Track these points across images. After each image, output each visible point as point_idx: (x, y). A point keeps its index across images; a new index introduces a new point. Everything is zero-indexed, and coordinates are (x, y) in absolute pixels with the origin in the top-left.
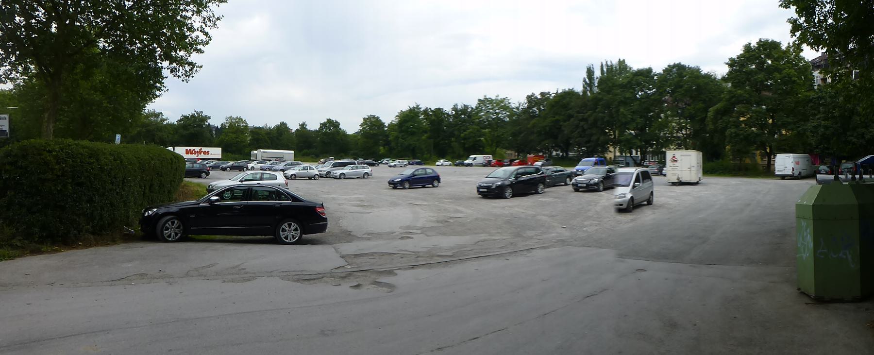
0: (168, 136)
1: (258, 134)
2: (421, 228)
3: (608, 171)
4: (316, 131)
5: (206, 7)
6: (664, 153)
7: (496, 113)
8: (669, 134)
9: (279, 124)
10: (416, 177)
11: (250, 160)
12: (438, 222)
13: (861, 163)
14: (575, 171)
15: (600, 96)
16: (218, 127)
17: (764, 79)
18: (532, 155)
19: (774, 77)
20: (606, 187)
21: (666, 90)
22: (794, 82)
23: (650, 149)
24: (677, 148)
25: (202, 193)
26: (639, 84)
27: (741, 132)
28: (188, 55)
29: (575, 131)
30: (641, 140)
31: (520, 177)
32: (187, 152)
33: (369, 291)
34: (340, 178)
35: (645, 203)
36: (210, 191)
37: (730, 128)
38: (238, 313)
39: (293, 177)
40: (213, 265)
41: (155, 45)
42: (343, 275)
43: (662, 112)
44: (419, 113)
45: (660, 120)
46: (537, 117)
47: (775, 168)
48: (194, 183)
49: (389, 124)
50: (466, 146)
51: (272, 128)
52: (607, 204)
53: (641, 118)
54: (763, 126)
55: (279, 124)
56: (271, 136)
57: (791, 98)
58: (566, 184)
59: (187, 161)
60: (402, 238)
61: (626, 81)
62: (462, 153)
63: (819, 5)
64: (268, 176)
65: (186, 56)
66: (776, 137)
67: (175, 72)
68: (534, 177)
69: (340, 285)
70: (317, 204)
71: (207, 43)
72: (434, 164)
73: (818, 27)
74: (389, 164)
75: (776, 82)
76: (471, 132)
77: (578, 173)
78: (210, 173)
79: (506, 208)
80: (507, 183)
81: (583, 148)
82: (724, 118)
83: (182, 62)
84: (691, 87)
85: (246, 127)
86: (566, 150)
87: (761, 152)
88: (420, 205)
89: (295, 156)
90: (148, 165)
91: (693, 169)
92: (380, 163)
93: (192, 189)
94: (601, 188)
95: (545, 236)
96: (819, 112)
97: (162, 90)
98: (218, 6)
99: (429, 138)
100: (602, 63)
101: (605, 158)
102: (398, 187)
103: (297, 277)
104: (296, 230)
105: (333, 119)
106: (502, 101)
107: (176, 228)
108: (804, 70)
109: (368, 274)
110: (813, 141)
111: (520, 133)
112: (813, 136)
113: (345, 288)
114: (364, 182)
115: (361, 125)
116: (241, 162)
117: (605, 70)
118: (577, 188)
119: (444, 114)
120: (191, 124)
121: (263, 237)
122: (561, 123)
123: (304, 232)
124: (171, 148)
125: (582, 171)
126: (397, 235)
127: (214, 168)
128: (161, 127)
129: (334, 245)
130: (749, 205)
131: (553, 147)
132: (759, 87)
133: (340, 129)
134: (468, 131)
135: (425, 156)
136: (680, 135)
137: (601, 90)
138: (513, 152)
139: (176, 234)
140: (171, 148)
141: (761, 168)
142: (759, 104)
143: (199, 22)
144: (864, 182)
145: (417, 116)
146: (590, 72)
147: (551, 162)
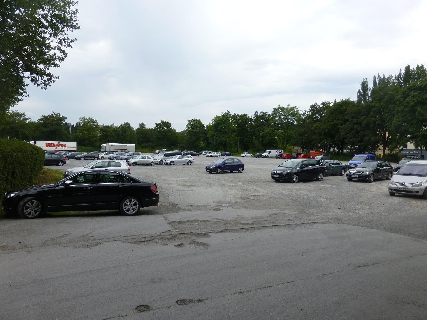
0: (30, 133)
1: (107, 131)
2: (229, 203)
3: (378, 166)
4: (152, 129)
5: (62, 31)
7: (286, 118)
9: (124, 124)
10: (226, 165)
11: (100, 151)
14: (349, 164)
15: (373, 104)
16: (73, 125)
18: (314, 151)
20: (375, 179)
25: (59, 178)
28: (46, 68)
29: (350, 133)
31: (304, 167)
32: (47, 145)
33: (189, 248)
34: (170, 165)
36: (65, 176)
38: (87, 272)
39: (135, 164)
40: (66, 235)
41: (18, 59)
42: (170, 237)
46: (319, 121)
48: (52, 170)
49: (207, 126)
50: (264, 142)
51: (118, 127)
52: (377, 192)
55: (124, 124)
56: (118, 133)
58: (341, 175)
59: (46, 153)
60: (215, 210)
62: (260, 148)
64: (114, 164)
65: (45, 68)
67: (35, 81)
68: (317, 167)
69: (167, 244)
70: (151, 184)
71: (63, 59)
72: (240, 156)
74: (207, 155)
76: (268, 132)
77: (351, 166)
78: (67, 162)
79: (293, 190)
80: (294, 171)
83: (41, 73)
85: (97, 126)
88: (229, 186)
89: (137, 148)
90: (11, 156)
92: (200, 154)
93: (50, 175)
94: (372, 179)
95: (323, 214)
97: (24, 95)
98: (72, 31)
99: (235, 136)
100: (375, 76)
101: (376, 155)
102: (213, 172)
103: (135, 240)
104: (135, 204)
105: (166, 120)
106: (292, 109)
107: (35, 207)
109: (189, 236)
111: (305, 134)
113: (171, 246)
114: (187, 168)
115: (187, 126)
116: (93, 153)
117: (377, 82)
118: (350, 178)
119: (248, 118)
120: (50, 122)
121: (110, 211)
122: (338, 127)
123: (141, 205)
124: (32, 143)
125: (355, 164)
126: (211, 208)
127: (70, 158)
128: (24, 125)
129: (165, 215)
133: (171, 128)
134: (265, 131)
137: (373, 99)
138: (299, 148)
139: (36, 212)
140: (32, 143)
143: (56, 42)
145: (227, 119)
146: (364, 85)
147: (329, 156)
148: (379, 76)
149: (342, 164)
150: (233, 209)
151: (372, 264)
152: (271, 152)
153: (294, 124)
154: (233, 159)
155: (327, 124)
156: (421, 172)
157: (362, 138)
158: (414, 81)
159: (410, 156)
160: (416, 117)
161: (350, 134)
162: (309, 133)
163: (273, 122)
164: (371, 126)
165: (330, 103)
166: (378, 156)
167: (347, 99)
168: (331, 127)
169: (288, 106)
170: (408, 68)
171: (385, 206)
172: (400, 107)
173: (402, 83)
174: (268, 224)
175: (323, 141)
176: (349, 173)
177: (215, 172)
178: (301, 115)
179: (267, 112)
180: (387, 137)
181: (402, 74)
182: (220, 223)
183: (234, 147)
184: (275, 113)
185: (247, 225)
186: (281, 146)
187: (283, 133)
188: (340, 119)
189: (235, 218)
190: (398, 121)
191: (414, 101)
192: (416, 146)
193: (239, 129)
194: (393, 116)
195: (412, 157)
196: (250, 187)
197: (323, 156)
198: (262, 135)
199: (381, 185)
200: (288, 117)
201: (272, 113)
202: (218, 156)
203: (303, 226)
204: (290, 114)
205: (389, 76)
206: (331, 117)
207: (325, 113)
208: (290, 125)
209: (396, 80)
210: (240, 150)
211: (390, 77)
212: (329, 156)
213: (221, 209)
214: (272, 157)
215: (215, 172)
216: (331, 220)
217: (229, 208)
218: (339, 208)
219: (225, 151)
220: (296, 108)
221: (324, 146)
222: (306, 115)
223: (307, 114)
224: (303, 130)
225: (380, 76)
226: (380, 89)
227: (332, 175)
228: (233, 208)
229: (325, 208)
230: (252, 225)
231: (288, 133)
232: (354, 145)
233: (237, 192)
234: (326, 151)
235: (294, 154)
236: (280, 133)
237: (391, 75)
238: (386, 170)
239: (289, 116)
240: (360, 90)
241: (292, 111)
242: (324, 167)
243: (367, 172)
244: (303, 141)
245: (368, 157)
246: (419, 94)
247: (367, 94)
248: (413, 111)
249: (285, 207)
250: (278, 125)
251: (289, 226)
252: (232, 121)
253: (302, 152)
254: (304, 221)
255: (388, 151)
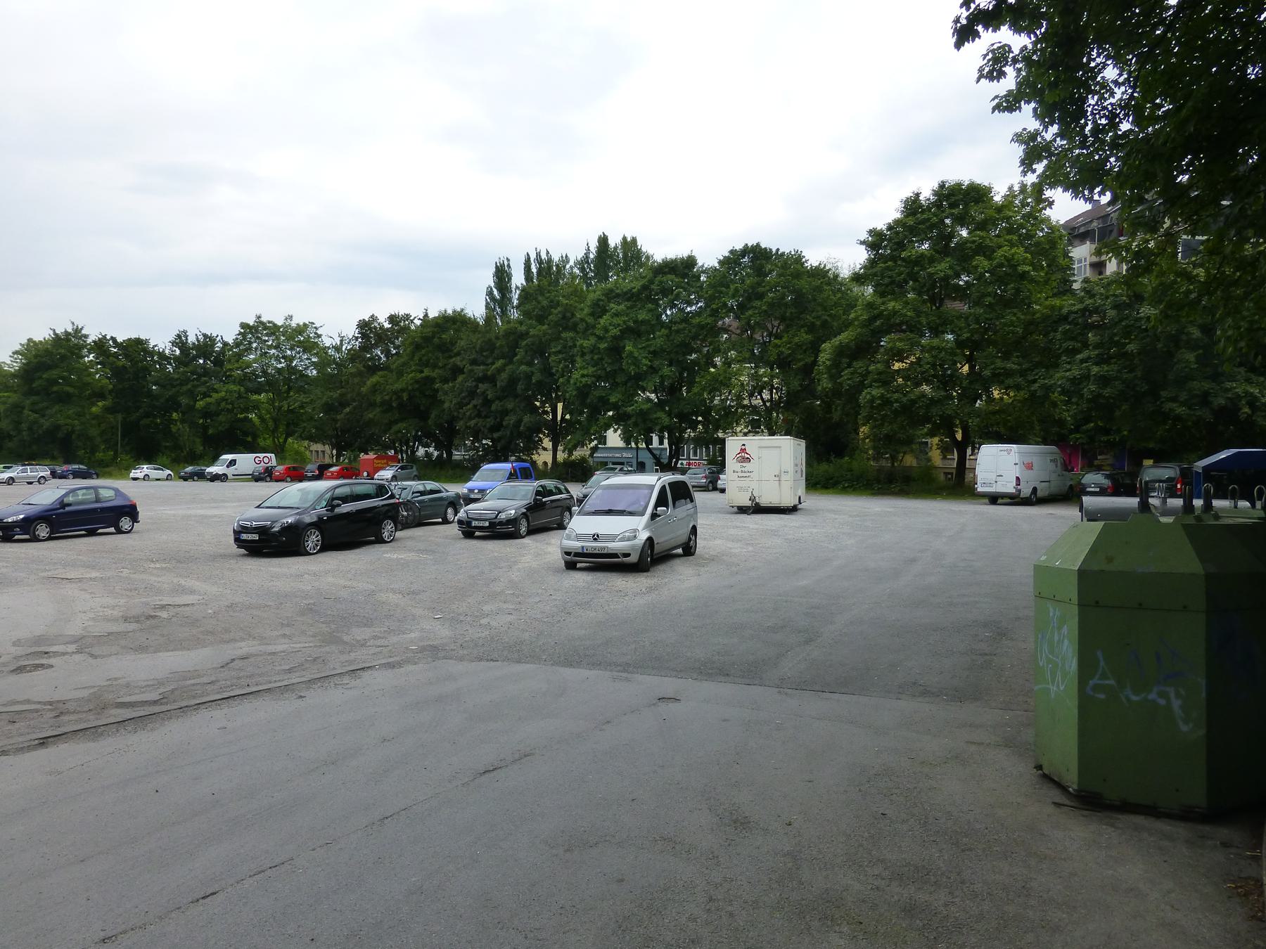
2: (76, 640)
3: (538, 493)
6: (723, 442)
8: (732, 400)
10: (67, 509)
12: (126, 619)
13: (1205, 468)
14: (465, 491)
15: (524, 328)
17: (950, 272)
18: (372, 455)
19: (976, 267)
20: (531, 528)
21: (725, 305)
22: (1024, 276)
23: (689, 433)
24: (750, 432)
26: (665, 292)
27: (896, 396)
29: (469, 404)
30: (669, 414)
31: (339, 505)
35: (680, 551)
37: (871, 386)
43: (717, 351)
44: (81, 347)
45: (712, 370)
46: (382, 369)
47: (975, 477)
50: (211, 431)
53: (670, 365)
54: (947, 382)
57: (1015, 314)
58: (446, 521)
60: (20, 670)
61: (638, 285)
63: (1094, 93)
66: (977, 405)
68: (376, 504)
72: (125, 476)
73: (1093, 144)
75: (980, 277)
76: (223, 399)
80: (308, 519)
81: (484, 442)
82: (858, 364)
84: (783, 297)
86: (446, 444)
87: (941, 441)
88: (80, 580)
91: (784, 477)
94: (523, 530)
95: (394, 639)
96: (1086, 345)
99: (107, 410)
101: (534, 463)
102: (16, 537)
106: (301, 329)
108: (1047, 247)
110: (1068, 415)
112: (1067, 403)
117: (534, 270)
118: (468, 530)
119: (152, 353)
125: (482, 491)
130: (913, 560)
131: (417, 438)
132: (939, 291)
134: (215, 395)
135: (99, 455)
136: (757, 402)
137: (526, 314)
138: (327, 448)
141: (942, 477)
142: (937, 331)
144: (1217, 517)
145: (73, 353)
146: (502, 274)
147: (414, 471)
148: (538, 254)
149: (448, 491)
150: (91, 660)
151: (514, 761)
152: (235, 461)
153: (307, 376)
154: (95, 488)
155: (405, 378)
156: (633, 504)
157: (498, 420)
158: (618, 276)
159: (614, 464)
160: (624, 367)
161: (468, 407)
162: (354, 404)
163: (240, 367)
164: (519, 387)
165: (412, 318)
166: (541, 467)
167: (459, 310)
168: (417, 386)
169: (286, 319)
170: (603, 241)
171: (554, 597)
172: (588, 340)
173: (590, 279)
174: (218, 693)
175: (395, 428)
176: (465, 515)
177: (27, 537)
178: (330, 351)
179: (218, 336)
180: (559, 418)
181: (592, 256)
182: (35, 714)
183: (103, 447)
184: (245, 339)
185: (142, 708)
186: (269, 442)
187: (273, 403)
188: (440, 364)
189: (96, 689)
190: (583, 376)
191: (619, 325)
192: (627, 438)
193: (121, 386)
194: (573, 362)
195: (619, 467)
196: (160, 579)
197: (397, 471)
198: (205, 407)
199: (547, 544)
200: (289, 352)
201: (237, 339)
202: (42, 480)
203: (332, 684)
204: (294, 346)
205: (562, 257)
206: (416, 358)
207: (399, 346)
208: (296, 379)
209: (578, 269)
210: (123, 456)
211: (563, 261)
212: (414, 469)
213: (43, 665)
214: (240, 477)
215: (27, 537)
216: (412, 655)
217: (77, 657)
218: (436, 617)
219: (67, 462)
220: (314, 326)
221: (401, 441)
222: (346, 349)
223: (348, 348)
224: (336, 394)
225: (540, 256)
226: (540, 290)
227: (420, 524)
228: (92, 656)
229: (399, 621)
230: (161, 704)
231: (291, 404)
232: (480, 438)
233: (110, 601)
234: (404, 456)
235: (311, 468)
236: (263, 402)
237: (566, 256)
238: (559, 504)
239: (291, 349)
240: (491, 289)
241: (302, 336)
242: (397, 501)
243: (510, 510)
244: (337, 426)
245: (515, 471)
246: (628, 308)
247: (510, 299)
248: (616, 351)
249: (276, 633)
250: (257, 376)
251: (287, 691)
252: (92, 361)
253: (335, 461)
254: (334, 669)
255: (563, 452)
